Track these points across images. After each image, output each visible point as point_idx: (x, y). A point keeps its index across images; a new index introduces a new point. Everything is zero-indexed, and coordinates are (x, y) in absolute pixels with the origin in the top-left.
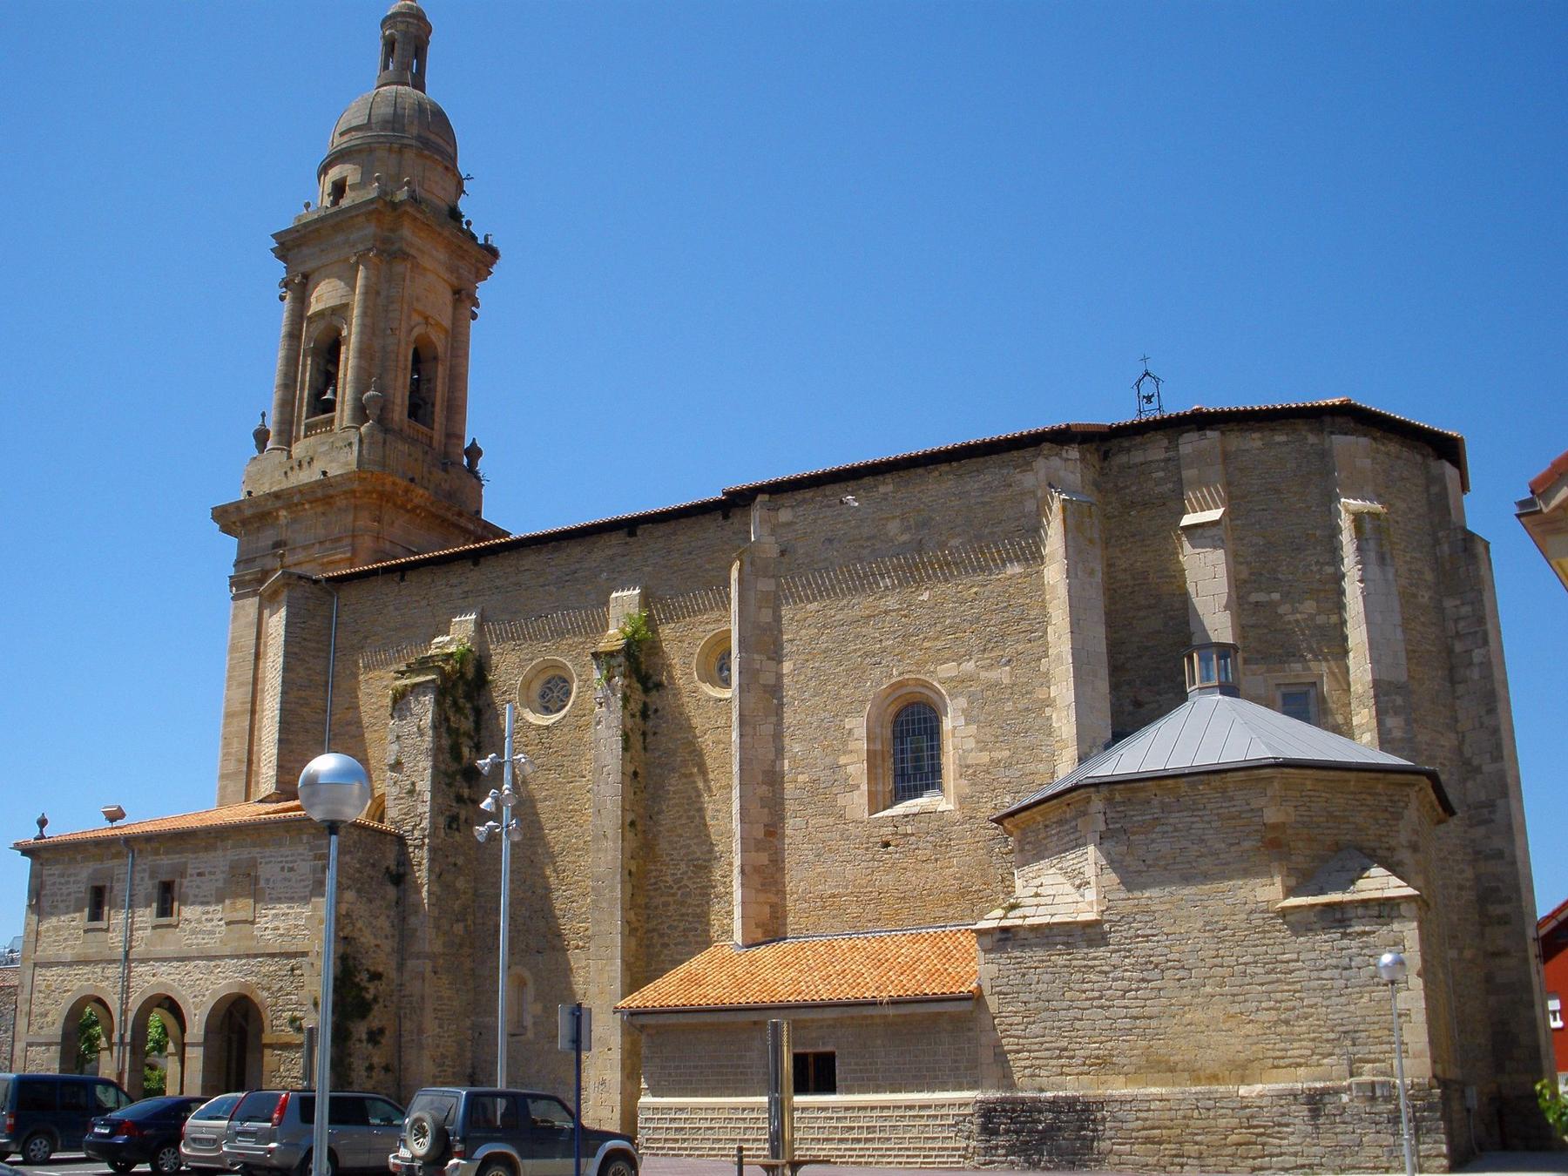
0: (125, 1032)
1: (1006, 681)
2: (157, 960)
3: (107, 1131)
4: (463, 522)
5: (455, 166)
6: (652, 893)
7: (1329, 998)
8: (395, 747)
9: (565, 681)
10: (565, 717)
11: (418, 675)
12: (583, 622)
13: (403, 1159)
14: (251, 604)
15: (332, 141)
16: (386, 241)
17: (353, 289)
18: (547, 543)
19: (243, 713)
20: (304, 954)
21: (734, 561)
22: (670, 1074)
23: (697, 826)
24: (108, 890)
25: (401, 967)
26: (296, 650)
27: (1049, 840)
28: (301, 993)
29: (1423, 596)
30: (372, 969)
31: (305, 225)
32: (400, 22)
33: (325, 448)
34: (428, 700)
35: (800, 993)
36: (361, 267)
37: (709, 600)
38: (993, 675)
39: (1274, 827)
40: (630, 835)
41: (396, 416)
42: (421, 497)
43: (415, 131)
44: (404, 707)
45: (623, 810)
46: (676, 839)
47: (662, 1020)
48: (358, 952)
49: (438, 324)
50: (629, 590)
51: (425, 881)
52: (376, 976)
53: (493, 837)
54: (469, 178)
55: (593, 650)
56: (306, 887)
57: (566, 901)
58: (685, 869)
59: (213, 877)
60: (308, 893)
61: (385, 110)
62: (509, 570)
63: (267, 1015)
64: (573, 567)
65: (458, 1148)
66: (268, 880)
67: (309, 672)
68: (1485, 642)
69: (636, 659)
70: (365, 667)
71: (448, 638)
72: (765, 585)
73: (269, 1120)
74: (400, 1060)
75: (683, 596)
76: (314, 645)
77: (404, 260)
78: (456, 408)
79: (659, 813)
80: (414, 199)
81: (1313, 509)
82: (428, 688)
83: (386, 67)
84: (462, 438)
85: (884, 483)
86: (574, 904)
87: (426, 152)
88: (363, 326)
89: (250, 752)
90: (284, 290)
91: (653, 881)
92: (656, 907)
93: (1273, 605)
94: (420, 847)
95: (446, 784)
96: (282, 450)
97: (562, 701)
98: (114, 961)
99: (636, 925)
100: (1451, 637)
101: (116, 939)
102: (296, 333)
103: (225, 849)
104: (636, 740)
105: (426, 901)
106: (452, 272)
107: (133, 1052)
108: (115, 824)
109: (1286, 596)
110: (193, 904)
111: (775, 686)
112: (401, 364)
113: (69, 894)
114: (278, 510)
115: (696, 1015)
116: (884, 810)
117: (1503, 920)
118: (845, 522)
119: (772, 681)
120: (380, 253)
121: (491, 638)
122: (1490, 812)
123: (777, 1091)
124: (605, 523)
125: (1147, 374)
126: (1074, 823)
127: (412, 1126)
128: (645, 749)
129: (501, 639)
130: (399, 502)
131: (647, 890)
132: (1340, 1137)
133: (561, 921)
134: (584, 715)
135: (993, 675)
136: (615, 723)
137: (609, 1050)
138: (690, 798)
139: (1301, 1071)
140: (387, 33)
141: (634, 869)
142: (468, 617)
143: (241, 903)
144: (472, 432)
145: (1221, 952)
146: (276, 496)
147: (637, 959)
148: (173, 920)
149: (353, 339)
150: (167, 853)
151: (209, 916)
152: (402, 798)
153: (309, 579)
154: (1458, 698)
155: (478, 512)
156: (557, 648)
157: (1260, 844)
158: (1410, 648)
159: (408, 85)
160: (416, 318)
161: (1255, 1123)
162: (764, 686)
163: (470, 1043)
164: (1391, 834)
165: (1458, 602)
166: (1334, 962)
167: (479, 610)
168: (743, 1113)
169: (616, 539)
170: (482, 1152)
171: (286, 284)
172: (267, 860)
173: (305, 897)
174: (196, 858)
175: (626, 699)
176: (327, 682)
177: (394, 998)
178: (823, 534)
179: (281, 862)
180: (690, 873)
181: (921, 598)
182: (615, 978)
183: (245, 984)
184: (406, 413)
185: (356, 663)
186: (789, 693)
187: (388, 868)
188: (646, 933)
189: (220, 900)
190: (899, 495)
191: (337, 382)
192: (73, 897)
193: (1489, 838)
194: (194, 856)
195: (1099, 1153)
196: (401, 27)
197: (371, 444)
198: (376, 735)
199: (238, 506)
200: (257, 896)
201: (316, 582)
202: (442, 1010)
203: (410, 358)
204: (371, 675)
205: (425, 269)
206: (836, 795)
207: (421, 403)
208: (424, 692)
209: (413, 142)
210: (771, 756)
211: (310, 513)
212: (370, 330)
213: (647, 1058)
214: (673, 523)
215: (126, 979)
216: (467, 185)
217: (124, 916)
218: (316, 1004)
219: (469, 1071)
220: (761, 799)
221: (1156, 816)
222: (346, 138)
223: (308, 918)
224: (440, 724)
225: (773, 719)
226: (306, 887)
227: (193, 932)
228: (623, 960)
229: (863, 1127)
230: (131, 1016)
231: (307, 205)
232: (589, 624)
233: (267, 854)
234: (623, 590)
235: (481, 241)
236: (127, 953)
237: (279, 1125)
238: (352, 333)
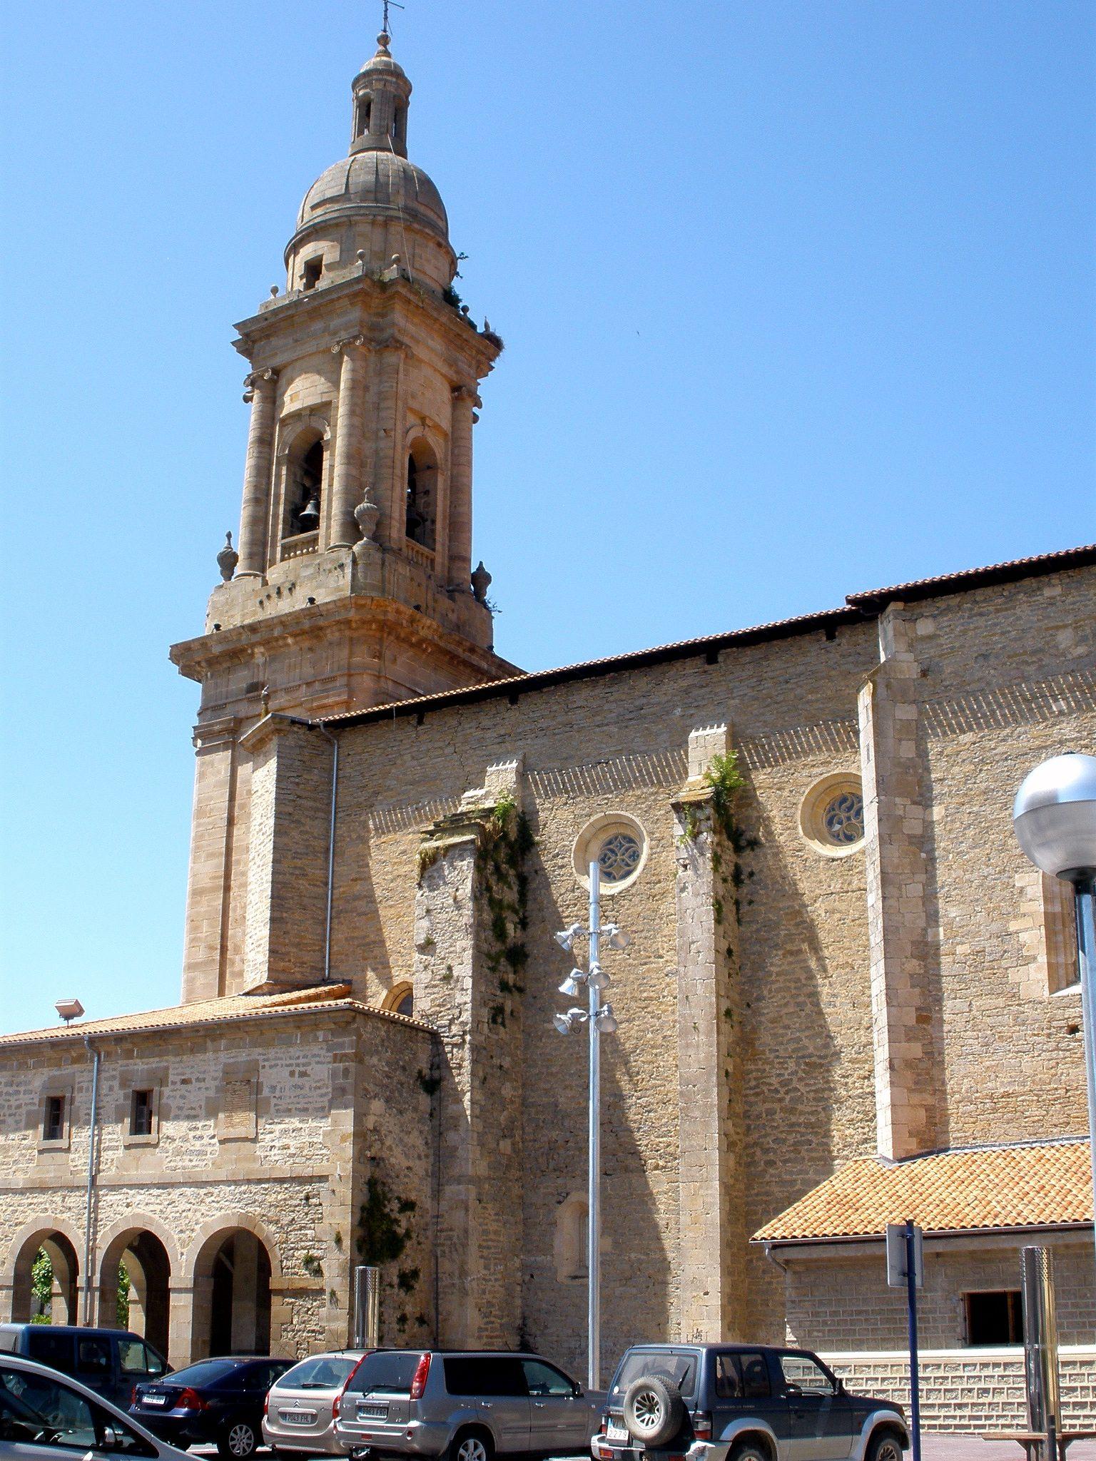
0: (93, 1273)
2: (131, 1187)
3: (162, 1402)
4: (475, 660)
5: (448, 243)
6: (752, 1099)
8: (425, 923)
9: (631, 841)
10: (635, 884)
11: (452, 835)
12: (654, 767)
13: (612, 1443)
14: (222, 759)
15: (301, 215)
16: (374, 328)
17: (336, 384)
18: (604, 675)
19: (213, 890)
20: (323, 1178)
21: (865, 683)
22: (825, 1323)
23: (808, 1016)
24: (67, 1102)
25: (437, 1194)
26: (290, 810)
28: (318, 1227)
30: (403, 1196)
31: (275, 312)
32: (376, 80)
33: (310, 571)
34: (466, 866)
35: (996, 1216)
36: (346, 358)
37: (815, 737)
40: (726, 1027)
41: (394, 534)
42: (429, 627)
43: (401, 201)
44: (436, 874)
45: (718, 996)
46: (781, 1031)
47: (816, 1253)
48: (388, 1175)
49: (437, 427)
50: (712, 727)
51: (467, 1087)
52: (408, 1206)
53: (579, 1029)
54: (463, 257)
55: (673, 801)
56: (322, 1096)
57: (641, 1110)
58: (794, 1068)
59: (202, 1084)
60: (326, 1104)
61: (364, 178)
62: (555, 708)
63: (275, 1256)
64: (637, 703)
65: (703, 1426)
66: (273, 1088)
67: (306, 837)
69: (726, 808)
70: (376, 829)
71: (482, 792)
72: (906, 712)
73: (407, 1390)
74: (437, 1309)
75: (781, 734)
76: (311, 804)
77: (397, 349)
78: (459, 526)
79: (759, 999)
80: (405, 278)
82: (465, 850)
83: (360, 132)
84: (467, 560)
85: (1049, 585)
86: (652, 1114)
87: (416, 226)
88: (351, 428)
89: (224, 937)
90: (250, 388)
91: (753, 1083)
92: (759, 1117)
94: (460, 1046)
95: (489, 968)
96: (255, 576)
97: (628, 865)
98: (78, 1188)
99: (735, 1137)
101: (79, 1161)
102: (267, 437)
103: (216, 1051)
104: (729, 908)
105: (468, 1112)
106: (450, 366)
107: (103, 1299)
108: (71, 1022)
110: (177, 1118)
111: (922, 836)
112: (398, 471)
113: (19, 1107)
114: (253, 646)
115: (982, 1239)
116: (1068, 985)
118: (1003, 633)
119: (918, 831)
120: (369, 340)
121: (538, 789)
123: (1037, 1342)
124: (638, 656)
127: (633, 1398)
128: (739, 921)
129: (550, 792)
130: (402, 635)
131: (746, 1096)
133: (637, 1135)
134: (659, 882)
136: (705, 889)
137: (706, 1293)
138: (799, 980)
140: (361, 93)
141: (730, 1069)
142: (507, 766)
143: (238, 1117)
144: (481, 553)
146: (253, 628)
147: (736, 1180)
148: (152, 1138)
149: (340, 444)
150: (141, 1057)
151: (198, 1133)
152: (435, 986)
153: (302, 724)
155: (491, 647)
156: (621, 801)
159: (389, 150)
160: (412, 419)
162: (910, 836)
163: (519, 1288)
167: (521, 757)
168: (1005, 1370)
169: (691, 669)
170: (732, 1431)
171: (253, 382)
172: (273, 1063)
173: (323, 1108)
174: (181, 1061)
175: (717, 860)
176: (328, 849)
177: (429, 1233)
178: (975, 649)
179: (291, 1065)
180: (801, 1074)
182: (712, 1204)
183: (246, 1216)
184: (404, 530)
185: (366, 827)
186: (941, 845)
187: (420, 1072)
188: (745, 1148)
189: (212, 1113)
190: (1070, 599)
191: (319, 495)
192: (24, 1110)
194: (178, 1059)
196: (379, 86)
197: (367, 565)
198: (392, 910)
199: (203, 642)
200: (260, 1108)
201: (312, 728)
202: (489, 1248)
203: (407, 465)
204: (384, 839)
205: (420, 361)
206: (1007, 969)
208: (460, 855)
209: (401, 214)
210: (922, 923)
211: (295, 648)
212: (358, 432)
213: (793, 1302)
214: (763, 646)
215: (94, 1209)
216: (461, 266)
217: (90, 1133)
218: (339, 1241)
219: (519, 1322)
220: (911, 976)
222: (319, 211)
223: (326, 1134)
224: (481, 894)
225: (923, 877)
226: (322, 1096)
227: (178, 1153)
228: (723, 1183)
229: (1088, 1388)
230: (100, 1255)
231: (275, 290)
232: (663, 771)
234: (704, 728)
235: (481, 329)
236: (93, 1179)
237: (420, 1396)
238: (338, 437)
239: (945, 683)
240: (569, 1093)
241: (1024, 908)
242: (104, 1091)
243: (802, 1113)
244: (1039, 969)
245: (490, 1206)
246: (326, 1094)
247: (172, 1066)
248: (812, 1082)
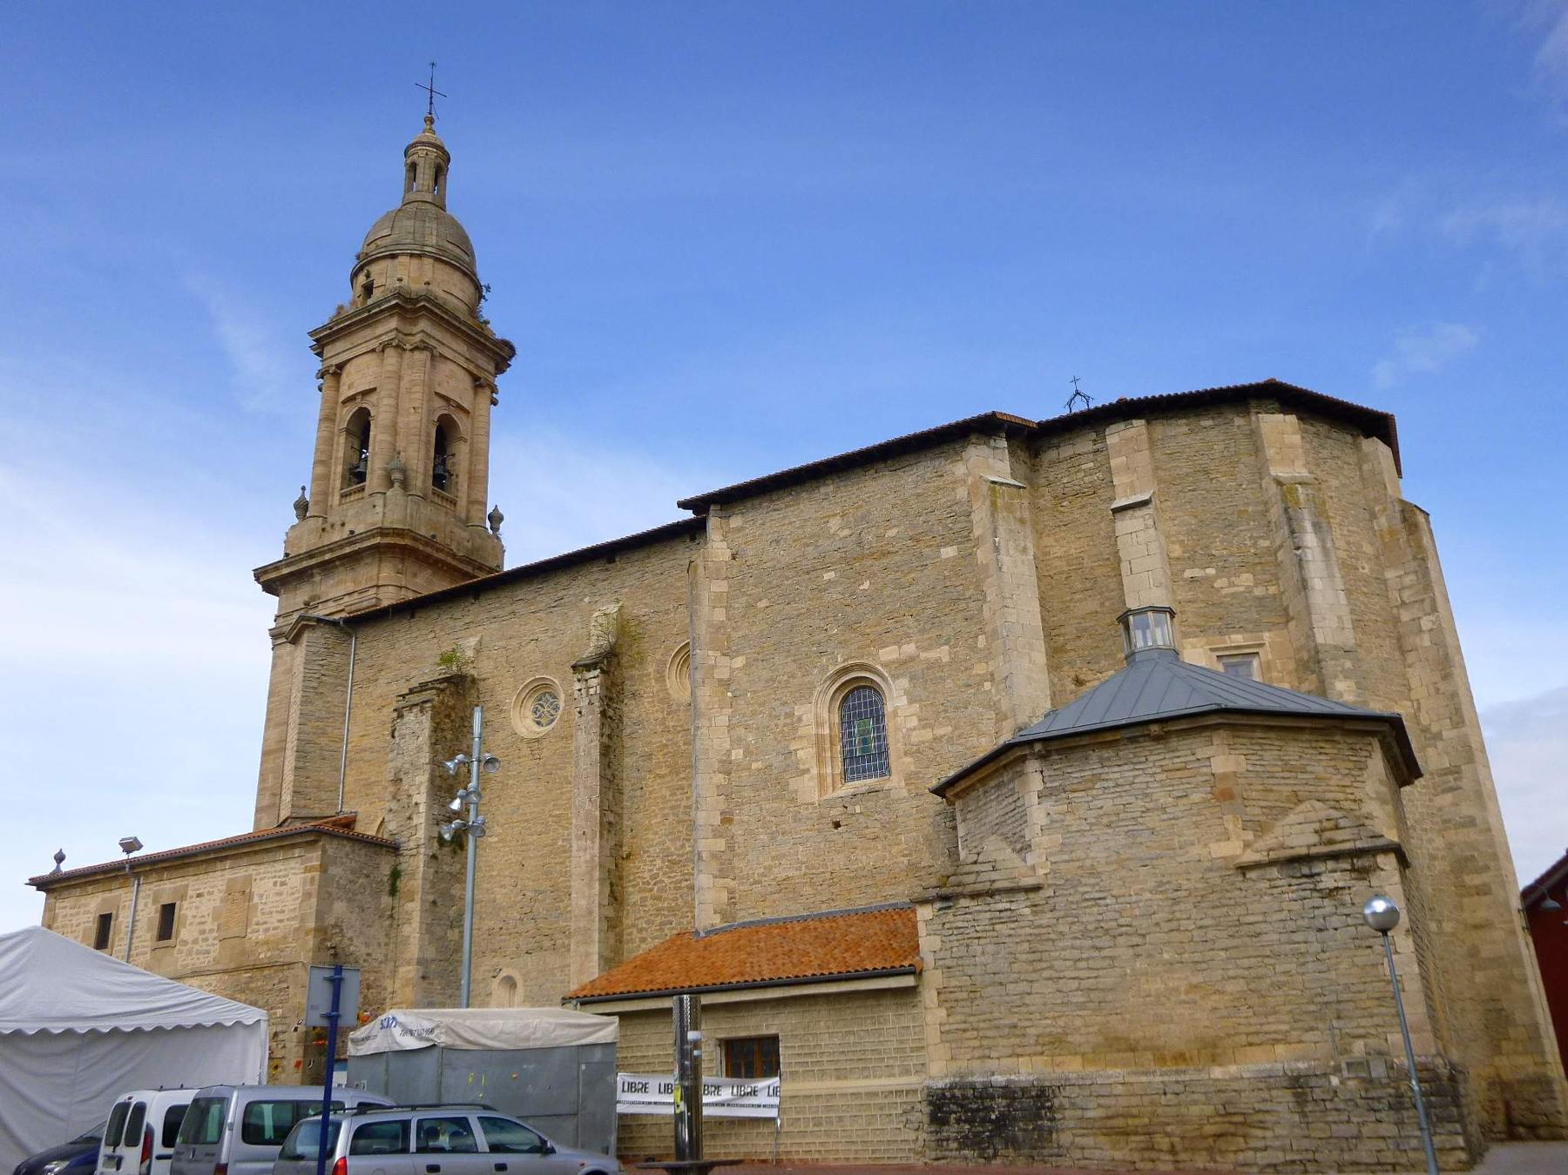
1: (946, 659)
7: (1303, 964)
24: (114, 917)
26: (315, 685)
27: (988, 806)
29: (1363, 568)
38: (932, 655)
39: (1225, 776)
64: (560, 594)
66: (261, 896)
68: (1434, 609)
78: (478, 479)
81: (1244, 486)
93: (1209, 580)
100: (1396, 606)
109: (1222, 570)
117: (1483, 891)
118: (790, 523)
122: (1455, 780)
125: (1078, 393)
126: (1011, 786)
132: (1334, 1127)
135: (932, 655)
139: (1280, 1049)
145: (1178, 915)
154: (1410, 666)
157: (1210, 796)
158: (1354, 617)
161: (1232, 1110)
162: (720, 680)
164: (1355, 785)
165: (1402, 573)
166: (1305, 923)
172: (262, 876)
181: (862, 588)
193: (1457, 805)
195: (1059, 1147)
199: (275, 566)
207: (447, 474)
220: (718, 787)
221: (1095, 772)
233: (262, 871)
239: (748, 563)
240: (504, 891)
241: (801, 732)
242: (140, 907)
243: (665, 899)
244: (811, 779)
245: (436, 982)
246: (298, 898)
247: (191, 884)
248: (672, 875)
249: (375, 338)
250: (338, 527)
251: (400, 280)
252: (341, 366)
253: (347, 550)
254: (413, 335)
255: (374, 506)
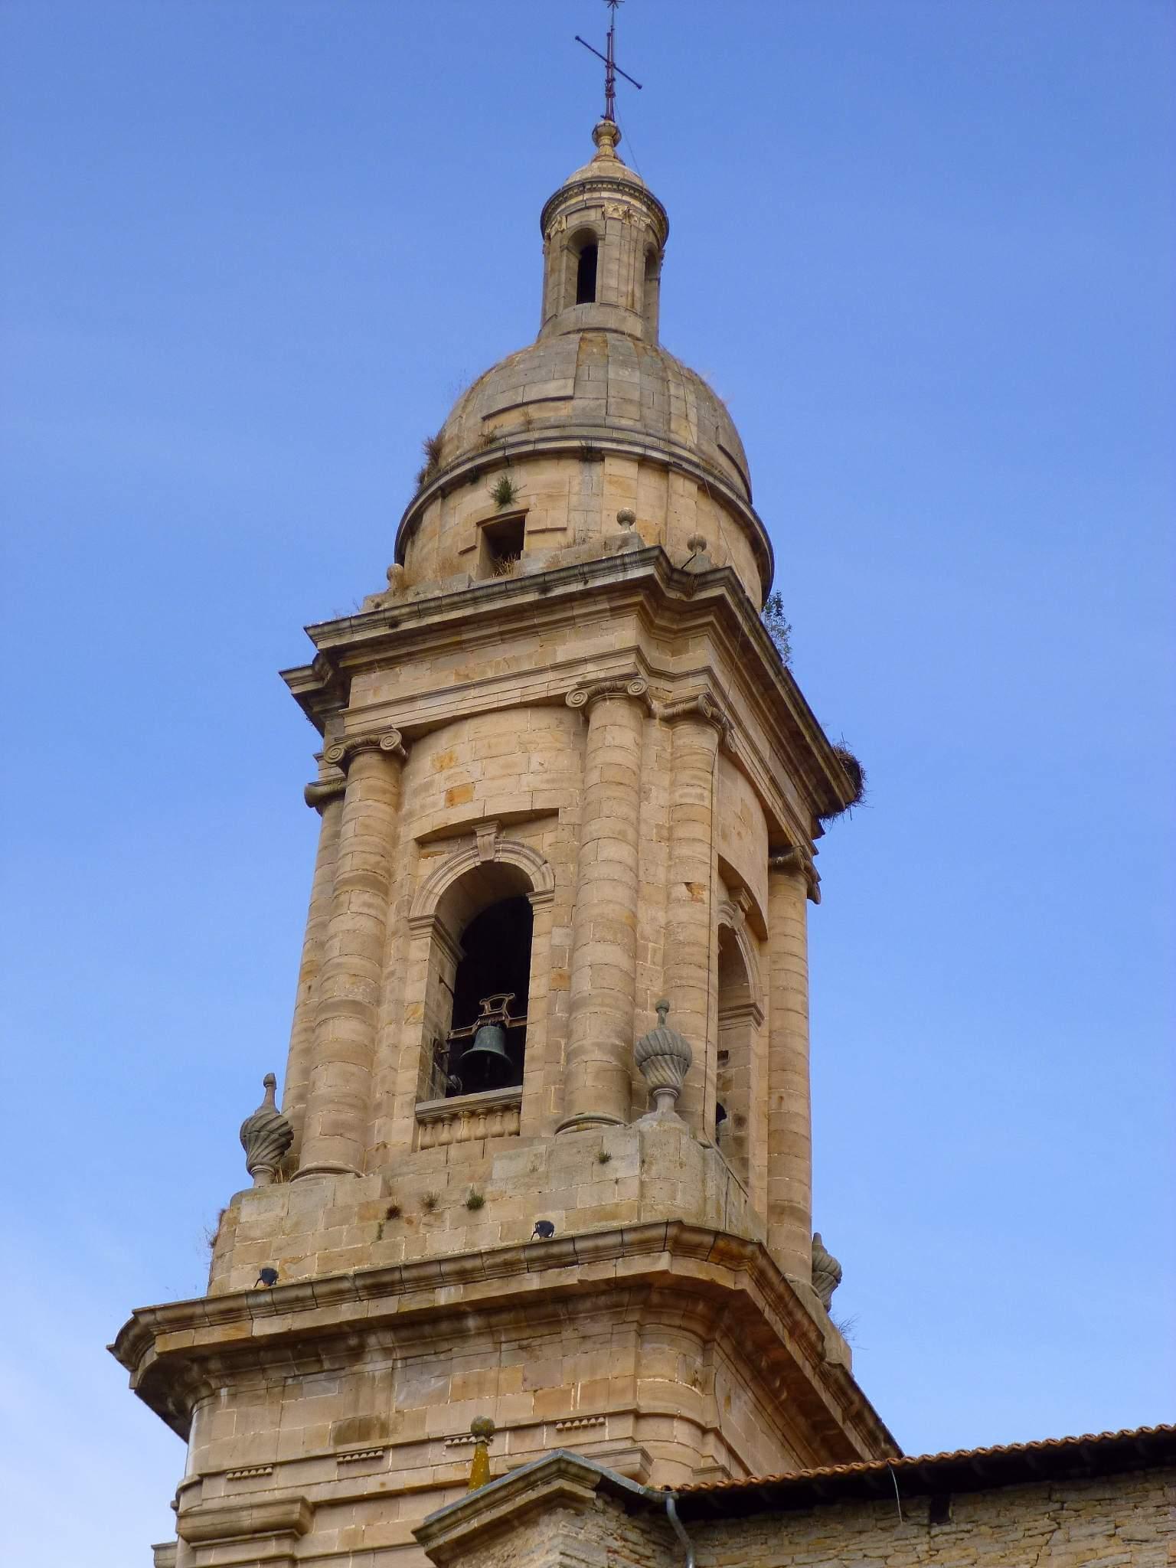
199: (181, 1316)
249: (555, 667)
250: (453, 1209)
251: (626, 519)
252: (415, 736)
253: (532, 1282)
254: (672, 678)
255: (604, 1159)
